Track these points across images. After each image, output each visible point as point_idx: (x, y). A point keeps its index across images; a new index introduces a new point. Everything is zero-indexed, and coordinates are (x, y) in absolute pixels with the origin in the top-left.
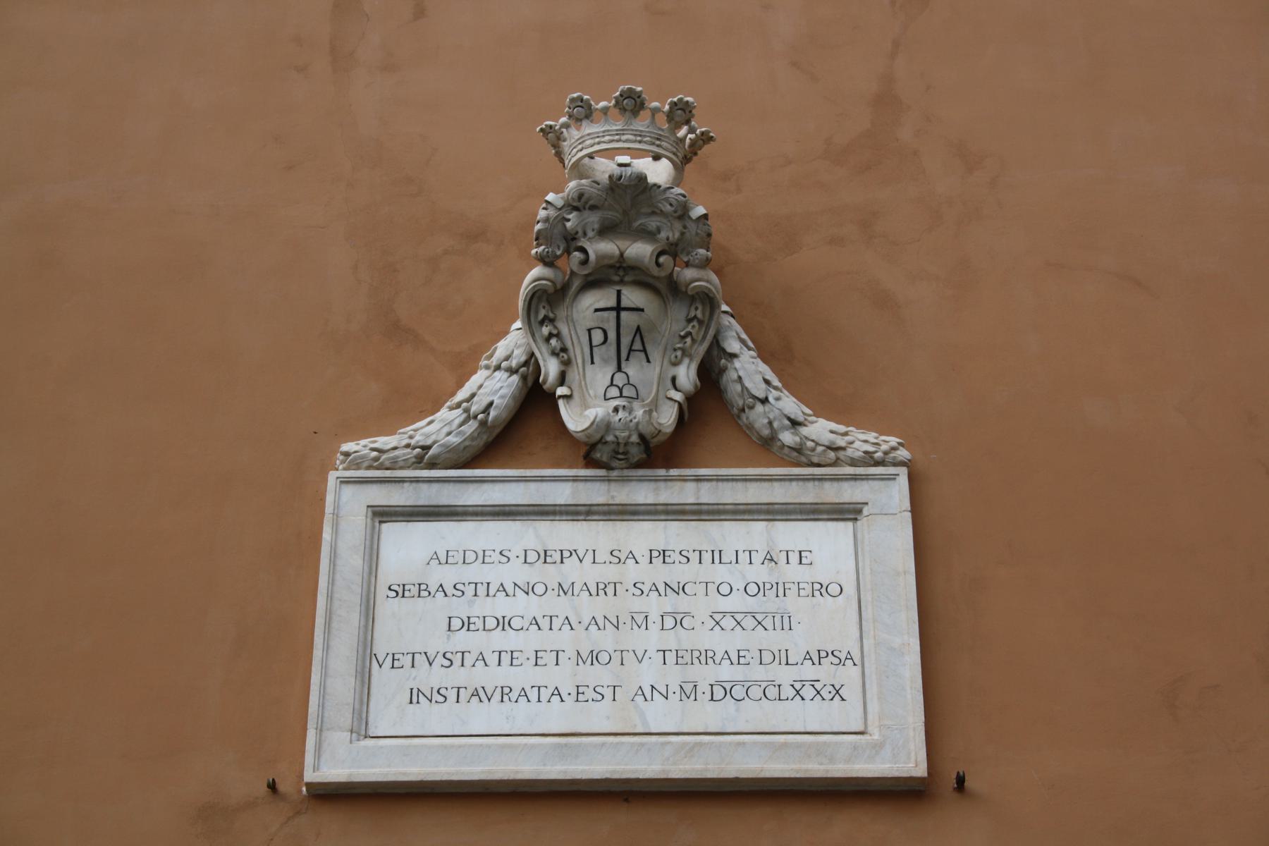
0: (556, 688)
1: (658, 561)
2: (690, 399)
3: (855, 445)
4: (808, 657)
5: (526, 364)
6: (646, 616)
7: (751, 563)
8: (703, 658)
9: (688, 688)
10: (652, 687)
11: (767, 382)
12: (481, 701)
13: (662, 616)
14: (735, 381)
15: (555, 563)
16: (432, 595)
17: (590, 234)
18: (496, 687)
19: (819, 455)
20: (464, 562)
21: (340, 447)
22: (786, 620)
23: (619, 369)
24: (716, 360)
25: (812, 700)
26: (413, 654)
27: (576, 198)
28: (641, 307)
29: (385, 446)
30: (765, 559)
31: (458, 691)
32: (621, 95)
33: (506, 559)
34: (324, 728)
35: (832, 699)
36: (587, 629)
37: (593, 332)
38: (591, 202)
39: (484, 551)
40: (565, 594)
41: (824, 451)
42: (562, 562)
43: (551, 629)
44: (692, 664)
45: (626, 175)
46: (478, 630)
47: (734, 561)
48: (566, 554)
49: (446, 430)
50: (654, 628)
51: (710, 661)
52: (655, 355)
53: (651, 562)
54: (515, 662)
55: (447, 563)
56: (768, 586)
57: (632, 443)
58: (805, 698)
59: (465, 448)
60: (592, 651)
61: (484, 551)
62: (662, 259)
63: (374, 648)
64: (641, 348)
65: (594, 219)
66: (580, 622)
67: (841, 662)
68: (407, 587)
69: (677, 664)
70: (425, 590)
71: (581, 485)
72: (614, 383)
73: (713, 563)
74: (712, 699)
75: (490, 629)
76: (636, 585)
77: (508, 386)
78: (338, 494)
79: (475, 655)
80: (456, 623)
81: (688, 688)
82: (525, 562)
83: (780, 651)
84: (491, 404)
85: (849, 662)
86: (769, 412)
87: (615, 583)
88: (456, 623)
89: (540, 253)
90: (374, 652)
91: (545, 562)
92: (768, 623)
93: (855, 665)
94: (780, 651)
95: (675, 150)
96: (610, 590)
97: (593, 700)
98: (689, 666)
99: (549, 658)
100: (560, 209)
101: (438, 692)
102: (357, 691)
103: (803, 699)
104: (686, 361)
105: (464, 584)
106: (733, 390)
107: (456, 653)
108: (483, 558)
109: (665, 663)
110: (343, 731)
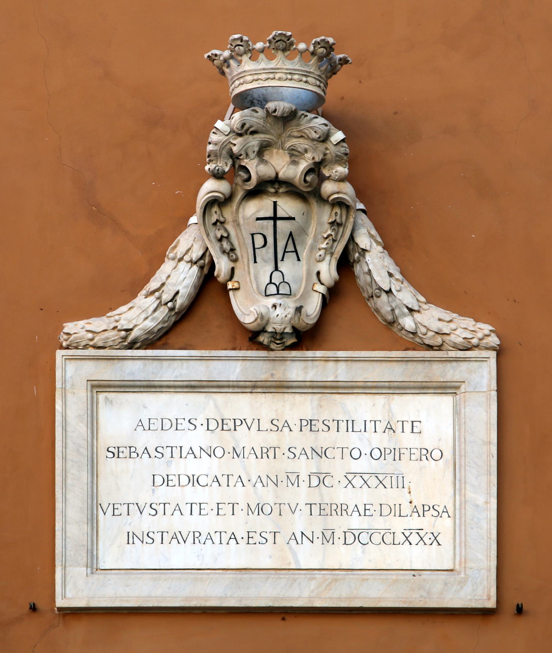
0: (233, 533)
1: (306, 429)
2: (330, 290)
3: (457, 332)
4: (415, 510)
5: (203, 255)
6: (298, 476)
7: (375, 432)
8: (339, 511)
9: (328, 534)
10: (302, 533)
11: (391, 275)
12: (179, 543)
13: (310, 476)
14: (367, 273)
15: (230, 430)
16: (140, 456)
17: (252, 155)
18: (190, 532)
19: (430, 339)
20: (162, 429)
21: (63, 328)
22: (400, 479)
23: (276, 269)
24: (352, 253)
25: (417, 544)
26: (128, 504)
27: (239, 128)
28: (293, 216)
29: (98, 328)
30: (386, 428)
31: (162, 535)
32: (274, 38)
33: (194, 427)
34: (67, 565)
35: (431, 544)
36: (254, 486)
37: (255, 236)
38: (251, 129)
39: (177, 419)
40: (238, 456)
41: (434, 336)
42: (235, 430)
43: (228, 486)
44: (331, 515)
45: (279, 109)
46: (175, 486)
47: (363, 430)
48: (238, 423)
49: (144, 316)
50: (304, 485)
51: (344, 513)
52: (304, 255)
53: (301, 430)
54: (203, 512)
55: (149, 429)
56: (388, 451)
57: (287, 333)
58: (412, 543)
59: (159, 330)
60: (258, 504)
61: (177, 419)
62: (309, 178)
63: (99, 498)
64: (294, 250)
65: (254, 142)
66: (249, 481)
67: (439, 515)
68: (121, 450)
69: (320, 515)
70: (134, 452)
71: (248, 363)
72: (273, 281)
73: (347, 431)
74: (345, 544)
75: (184, 485)
76: (291, 450)
77: (190, 277)
78: (64, 370)
79: (173, 506)
80: (158, 480)
81: (328, 534)
82: (208, 429)
83: (395, 505)
84: (177, 293)
85: (445, 514)
86: (392, 302)
87: (275, 448)
88: (158, 480)
89: (212, 171)
90: (99, 502)
91: (223, 429)
92: (387, 482)
93: (449, 517)
94: (395, 505)
95: (318, 83)
96: (271, 454)
97: (259, 543)
98: (329, 517)
99: (226, 509)
100: (227, 135)
101: (148, 535)
102: (89, 535)
103: (410, 544)
104: (328, 258)
105: (163, 447)
106: (362, 280)
107: (160, 504)
108: (176, 425)
109: (311, 515)
110: (81, 567)
